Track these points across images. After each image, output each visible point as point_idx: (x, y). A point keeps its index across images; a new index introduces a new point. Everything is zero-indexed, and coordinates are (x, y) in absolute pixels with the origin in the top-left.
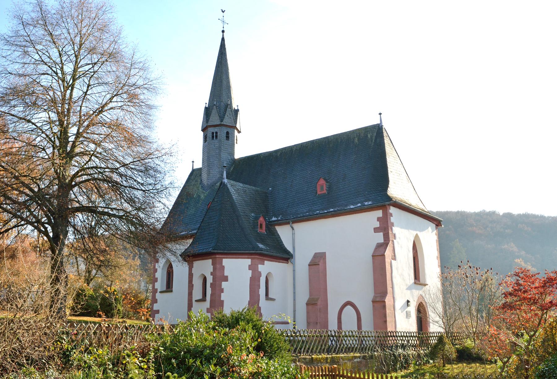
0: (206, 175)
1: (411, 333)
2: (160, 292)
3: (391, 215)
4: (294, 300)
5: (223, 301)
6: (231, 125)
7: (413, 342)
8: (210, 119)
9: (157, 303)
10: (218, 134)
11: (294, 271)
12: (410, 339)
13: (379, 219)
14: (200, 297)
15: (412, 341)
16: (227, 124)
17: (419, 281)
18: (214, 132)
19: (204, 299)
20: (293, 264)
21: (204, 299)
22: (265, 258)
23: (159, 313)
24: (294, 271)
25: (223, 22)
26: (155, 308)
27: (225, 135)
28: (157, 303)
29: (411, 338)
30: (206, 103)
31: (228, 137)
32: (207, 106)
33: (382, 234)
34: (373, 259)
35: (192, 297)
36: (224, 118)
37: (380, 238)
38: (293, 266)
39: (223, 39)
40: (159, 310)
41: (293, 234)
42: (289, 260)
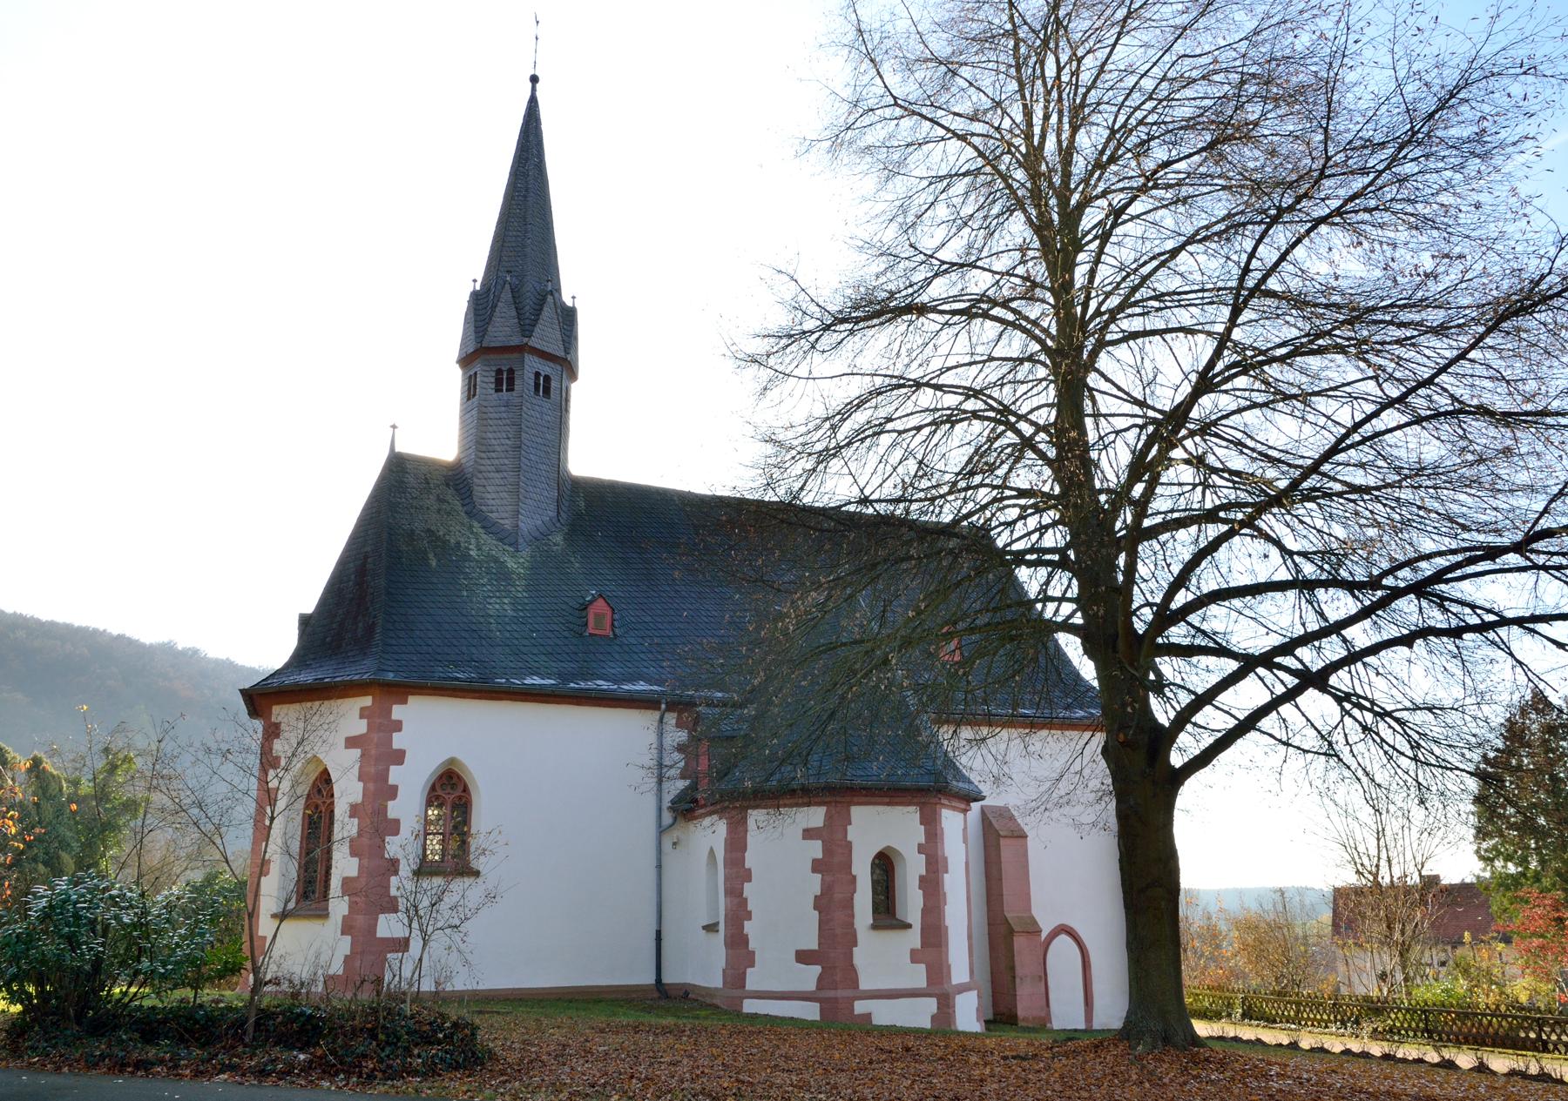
4: (659, 867)
30: (475, 281)
32: (478, 288)
35: (853, 916)
39: (533, 103)
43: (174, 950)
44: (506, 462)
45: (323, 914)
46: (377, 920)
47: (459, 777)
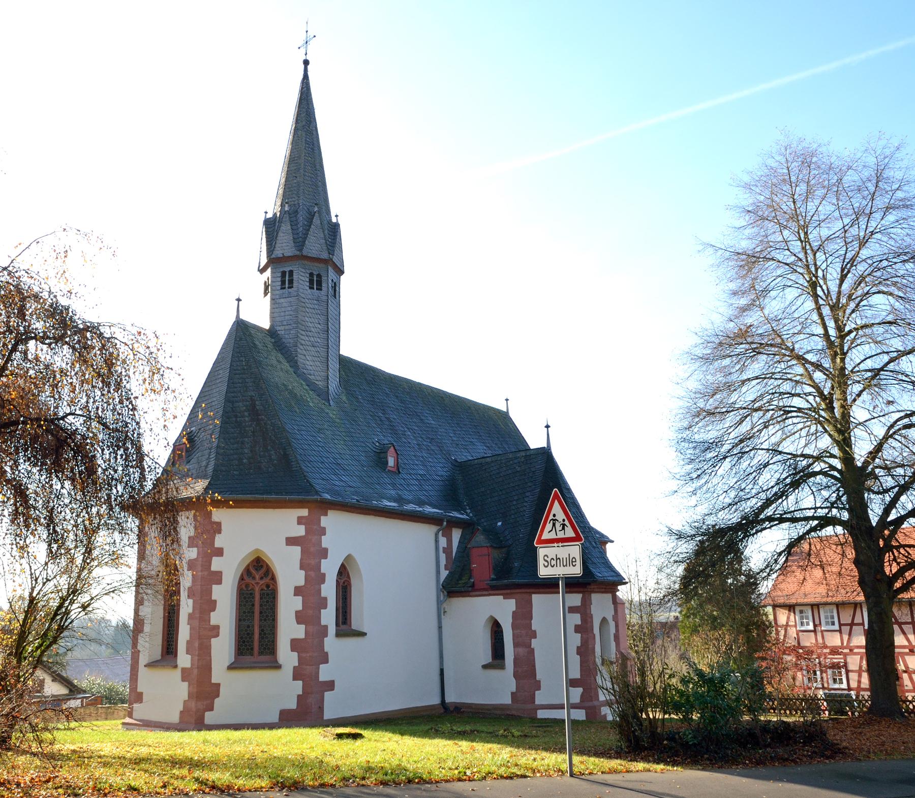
4: (440, 627)
5: (215, 602)
9: (326, 661)
23: (333, 690)
26: (323, 677)
28: (326, 661)
39: (306, 77)
40: (333, 682)
44: (319, 341)
45: (502, 667)
46: (318, 668)
47: (263, 561)
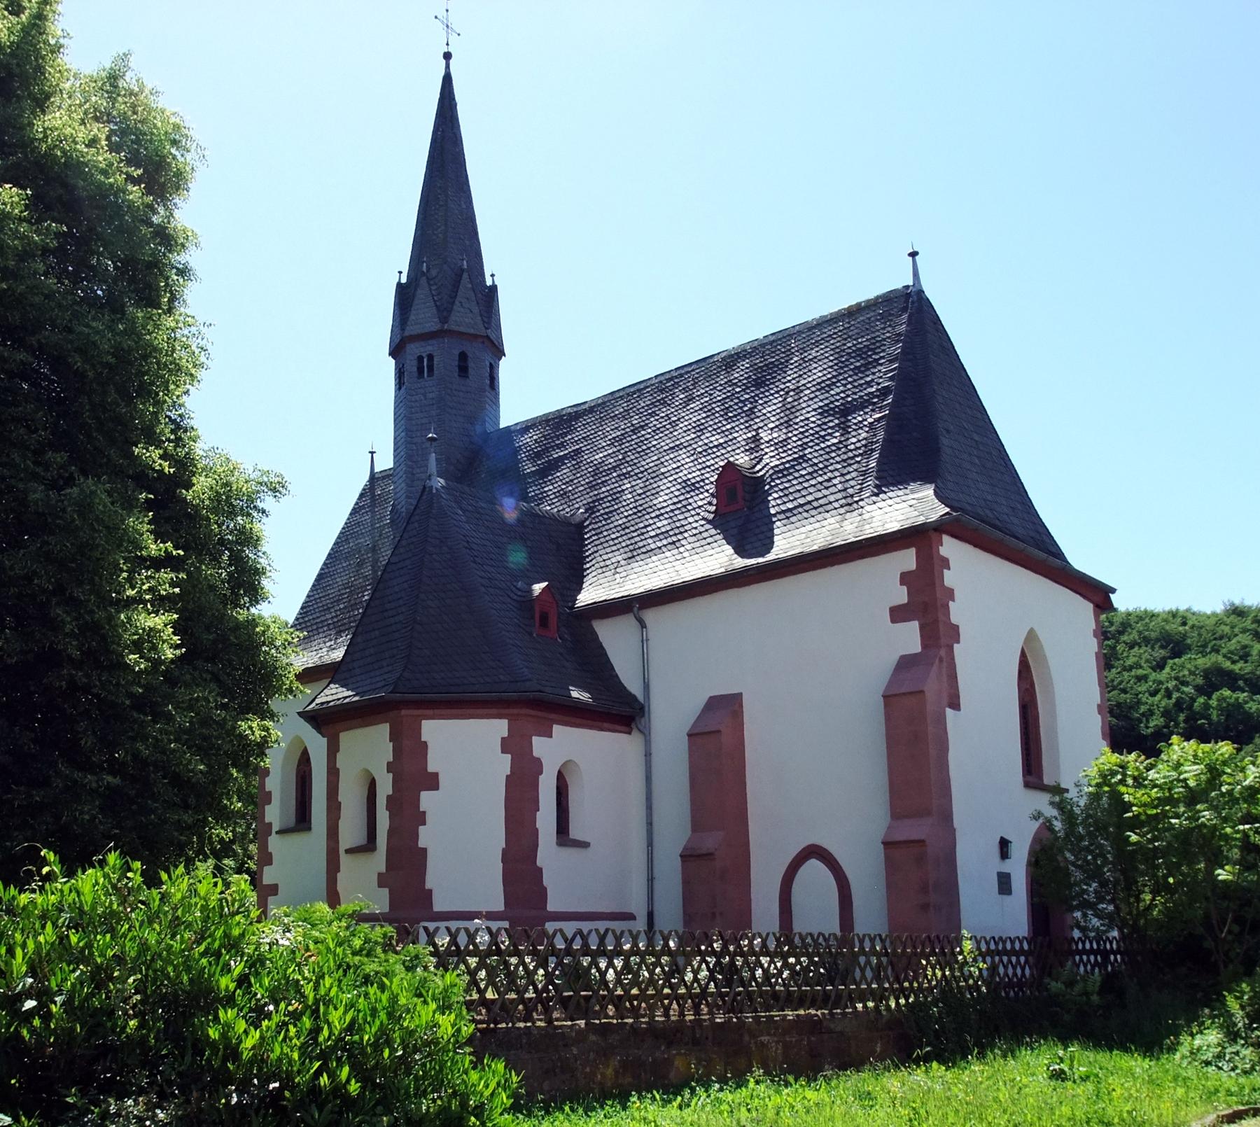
0: (403, 485)
1: (1004, 942)
2: (277, 833)
3: (945, 563)
5: (430, 891)
6: (472, 331)
7: (1010, 971)
8: (412, 317)
10: (436, 360)
11: (648, 755)
12: (1001, 961)
13: (905, 578)
14: (360, 838)
15: (1005, 967)
16: (462, 329)
17: (1040, 777)
18: (424, 355)
19: (369, 845)
20: (646, 735)
21: (369, 845)
22: (553, 716)
24: (648, 755)
25: (447, 26)
27: (457, 363)
29: (1005, 959)
30: (400, 273)
31: (463, 370)
32: (404, 280)
33: (915, 625)
34: (886, 705)
36: (450, 311)
37: (909, 637)
38: (646, 741)
39: (447, 80)
41: (644, 641)
42: (633, 725)
43: (603, 1002)
